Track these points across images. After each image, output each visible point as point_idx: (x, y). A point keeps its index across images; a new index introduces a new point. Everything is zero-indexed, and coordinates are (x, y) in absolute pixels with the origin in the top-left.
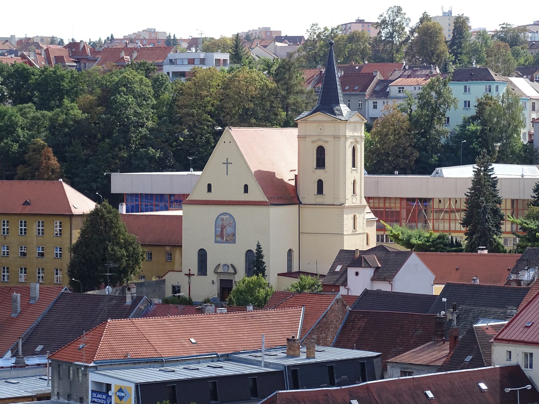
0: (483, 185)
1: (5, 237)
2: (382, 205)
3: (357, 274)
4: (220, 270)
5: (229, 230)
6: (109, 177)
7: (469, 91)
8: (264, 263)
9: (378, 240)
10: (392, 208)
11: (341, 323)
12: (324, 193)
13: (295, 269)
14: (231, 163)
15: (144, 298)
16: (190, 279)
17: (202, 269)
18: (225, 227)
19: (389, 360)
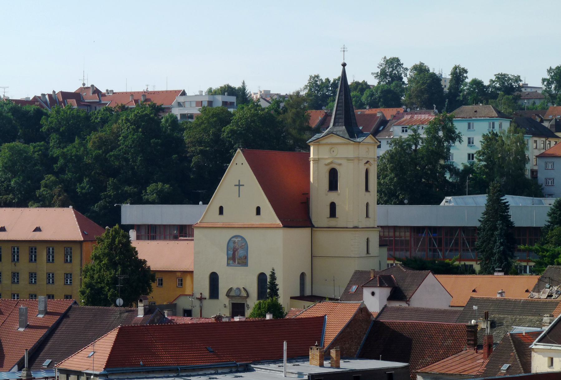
0: (497, 212)
1: (15, 264)
2: (391, 234)
3: (373, 294)
4: (232, 294)
5: (241, 253)
6: (119, 209)
7: (473, 128)
8: (277, 285)
9: (469, 159)
10: (401, 237)
11: (365, 334)
12: (337, 216)
13: (308, 293)
14: (239, 181)
15: (157, 310)
16: (201, 302)
17: (214, 293)
18: (237, 250)
19: (419, 371)
